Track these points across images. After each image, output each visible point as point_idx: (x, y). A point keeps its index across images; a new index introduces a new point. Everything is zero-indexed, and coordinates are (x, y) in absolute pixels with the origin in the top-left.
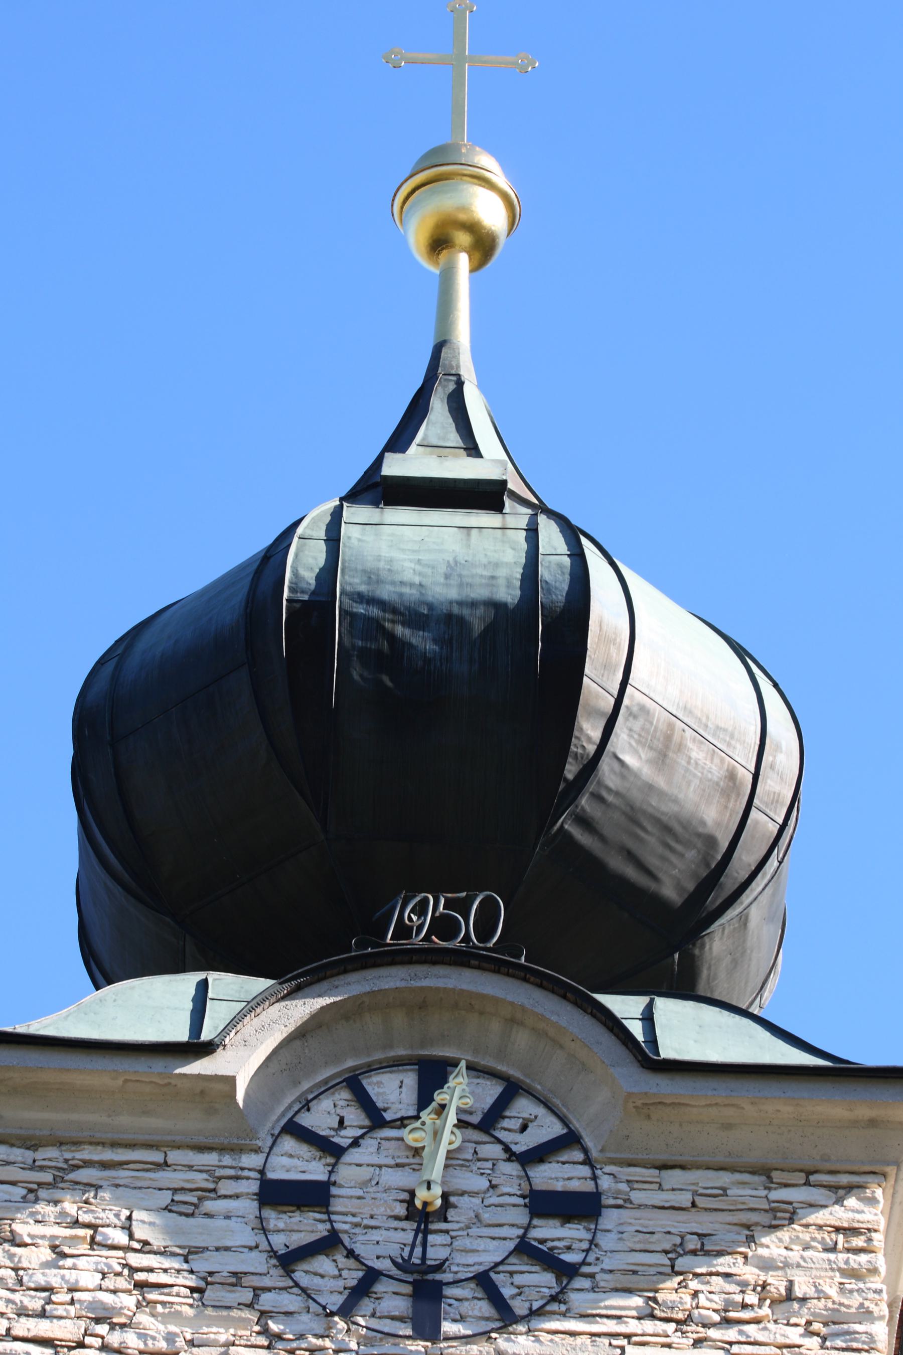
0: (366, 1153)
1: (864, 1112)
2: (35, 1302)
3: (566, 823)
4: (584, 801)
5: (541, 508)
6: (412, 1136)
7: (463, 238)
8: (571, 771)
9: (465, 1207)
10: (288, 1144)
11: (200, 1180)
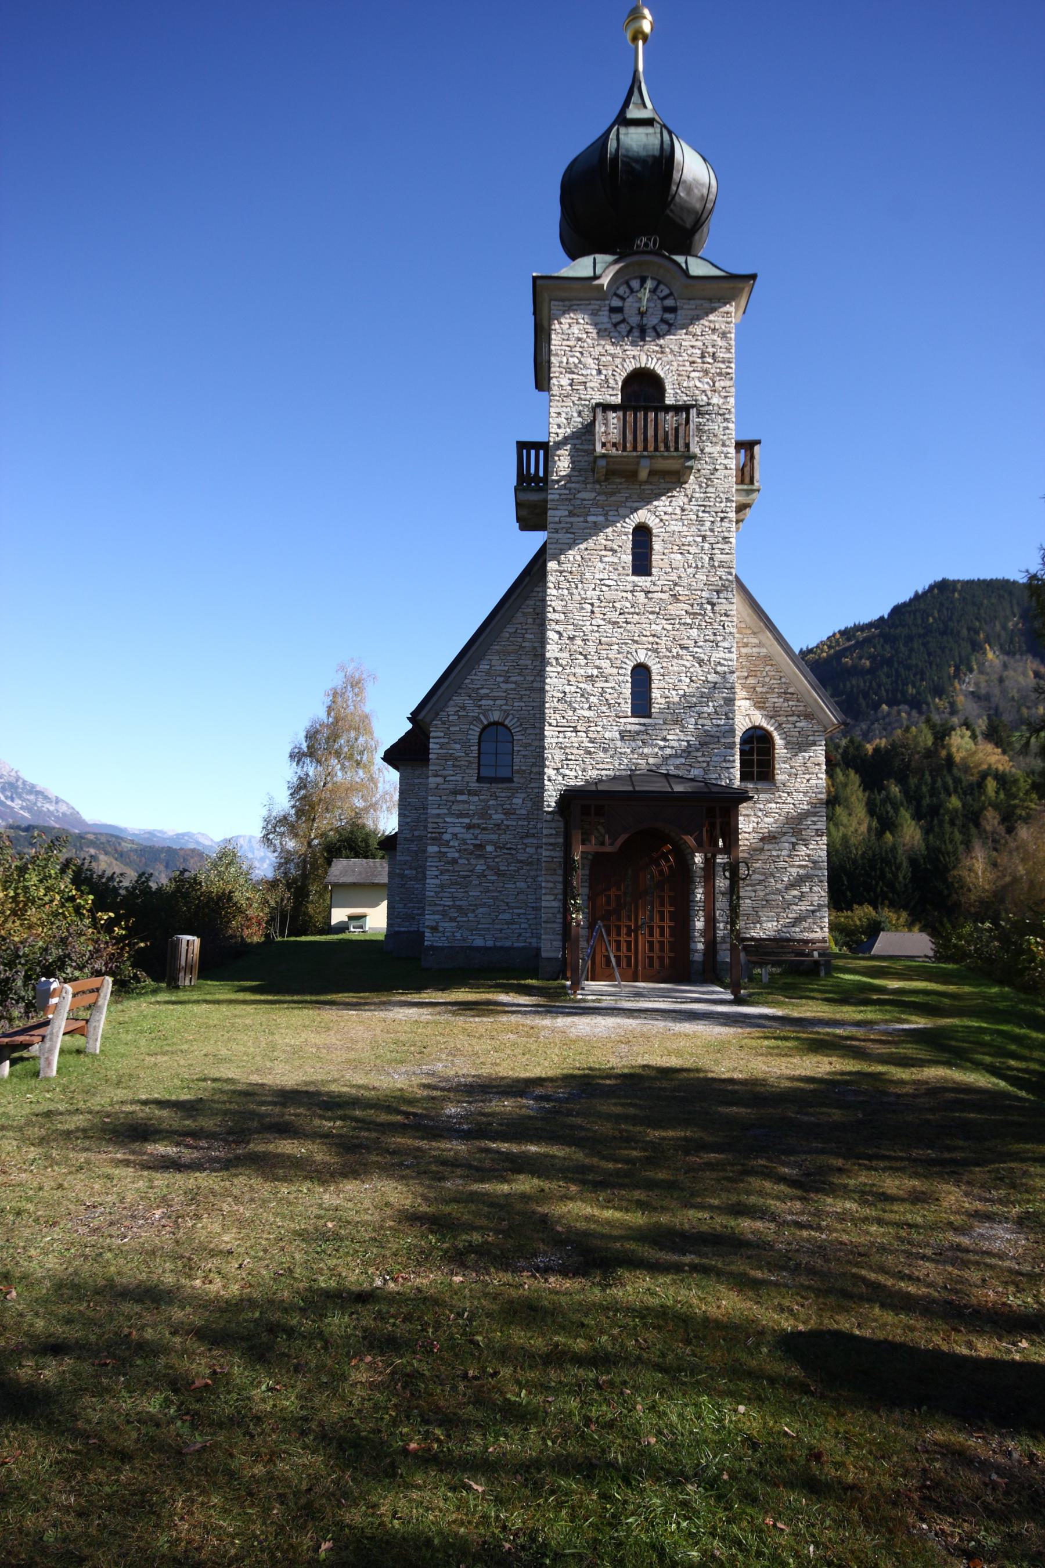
0: (630, 300)
1: (732, 285)
2: (566, 337)
3: (668, 212)
4: (672, 206)
5: (664, 126)
6: (639, 295)
7: (640, 36)
8: (669, 199)
9: (650, 311)
10: (615, 298)
11: (597, 307)
